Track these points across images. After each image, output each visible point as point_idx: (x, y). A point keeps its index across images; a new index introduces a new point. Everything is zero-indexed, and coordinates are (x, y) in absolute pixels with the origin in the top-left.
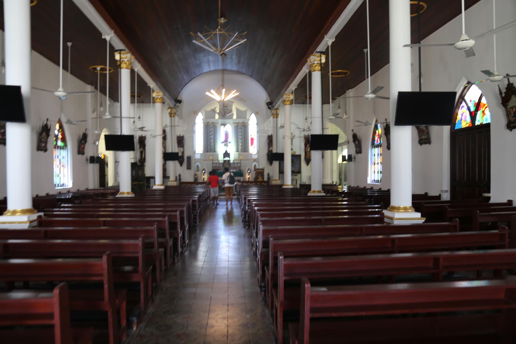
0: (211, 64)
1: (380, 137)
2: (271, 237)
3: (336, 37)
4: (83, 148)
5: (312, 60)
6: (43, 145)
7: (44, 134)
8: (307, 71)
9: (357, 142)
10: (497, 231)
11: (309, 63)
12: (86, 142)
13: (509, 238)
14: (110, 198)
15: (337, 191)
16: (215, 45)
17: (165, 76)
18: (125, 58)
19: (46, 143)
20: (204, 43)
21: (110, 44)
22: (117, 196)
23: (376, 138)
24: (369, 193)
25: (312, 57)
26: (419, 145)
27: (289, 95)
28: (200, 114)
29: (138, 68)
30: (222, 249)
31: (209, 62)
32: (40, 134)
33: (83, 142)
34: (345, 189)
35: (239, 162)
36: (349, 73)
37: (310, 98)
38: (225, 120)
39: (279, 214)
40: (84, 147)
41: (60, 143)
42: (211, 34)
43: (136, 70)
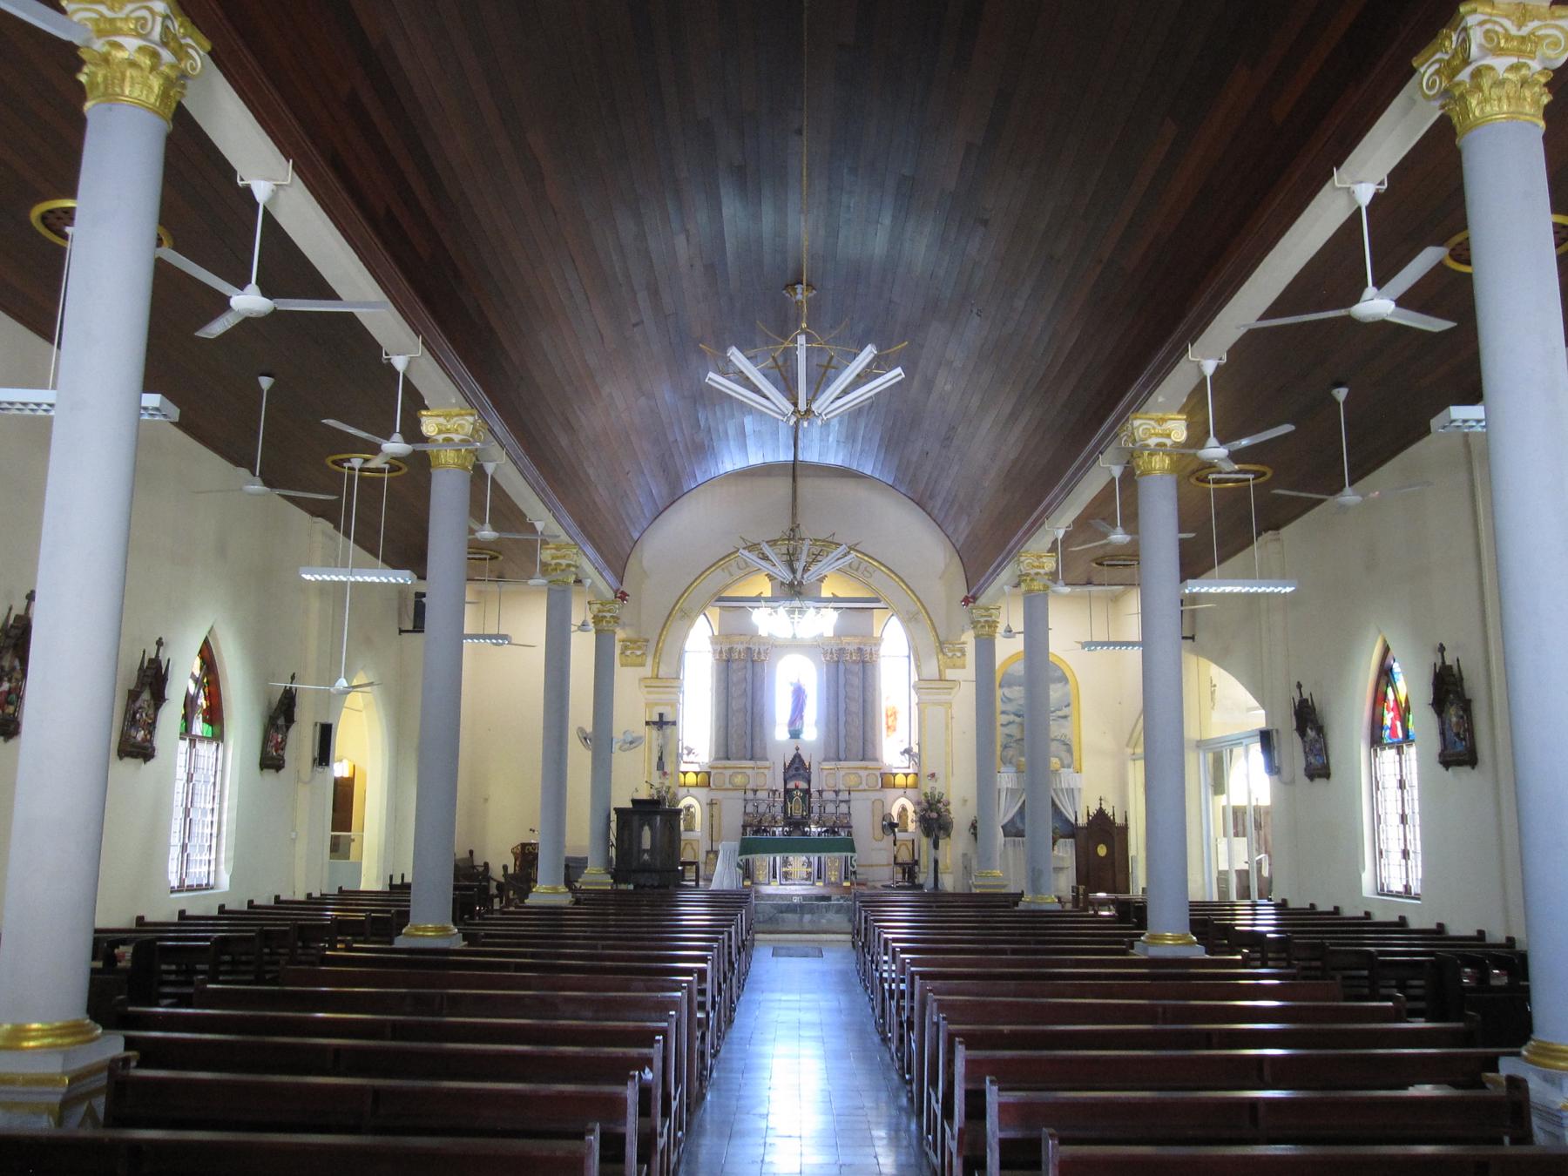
0: (750, 442)
1: (1403, 712)
2: (1052, 1136)
4: (281, 746)
6: (141, 735)
7: (146, 696)
8: (1117, 471)
10: (1461, 1025)
11: (1123, 440)
12: (290, 720)
14: (364, 949)
15: (1228, 930)
18: (450, 421)
19: (151, 727)
21: (407, 381)
22: (400, 942)
23: (1388, 718)
24: (1397, 949)
25: (1137, 423)
27: (1038, 553)
28: (701, 619)
29: (501, 465)
31: (742, 433)
32: (133, 696)
36: (1269, 475)
39: (1034, 1034)
40: (284, 740)
41: (199, 727)
43: (490, 468)
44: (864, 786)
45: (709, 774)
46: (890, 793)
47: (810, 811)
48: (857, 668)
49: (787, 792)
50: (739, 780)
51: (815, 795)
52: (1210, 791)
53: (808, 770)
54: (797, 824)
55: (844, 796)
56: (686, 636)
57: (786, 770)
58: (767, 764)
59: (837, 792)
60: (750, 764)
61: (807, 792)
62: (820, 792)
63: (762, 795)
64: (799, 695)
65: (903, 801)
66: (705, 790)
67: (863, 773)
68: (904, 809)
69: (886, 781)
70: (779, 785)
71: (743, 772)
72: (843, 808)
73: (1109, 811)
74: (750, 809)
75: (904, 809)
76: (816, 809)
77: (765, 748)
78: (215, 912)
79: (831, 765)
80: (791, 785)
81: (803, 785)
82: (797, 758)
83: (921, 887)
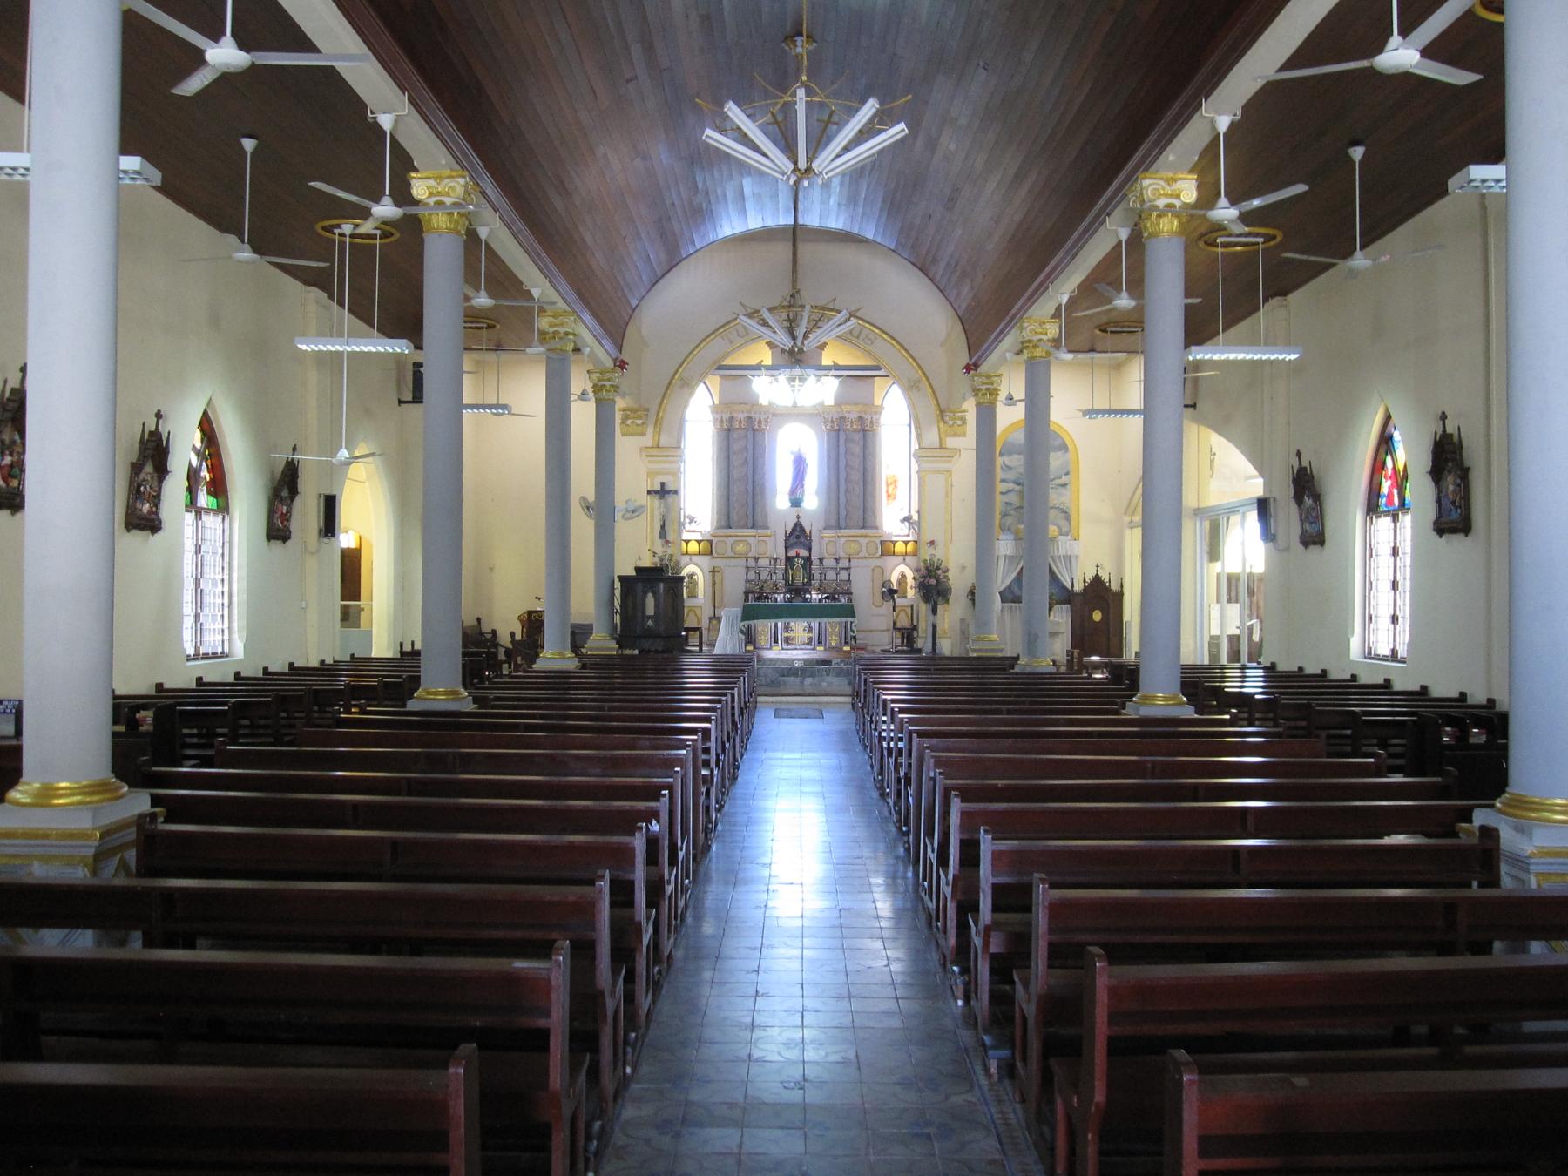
1: (1400, 481)
3: (1246, 108)
4: (286, 517)
5: (1148, 194)
7: (149, 468)
8: (1124, 234)
9: (1450, 483)
13: (1484, 949)
16: (789, 148)
17: (575, 267)
19: (156, 499)
20: (745, 140)
23: (1386, 486)
25: (1146, 183)
26: (1434, 535)
30: (804, 900)
33: (285, 493)
34: (1254, 685)
35: (1074, 532)
37: (632, 435)
38: (807, 414)
40: (289, 511)
42: (365, 214)
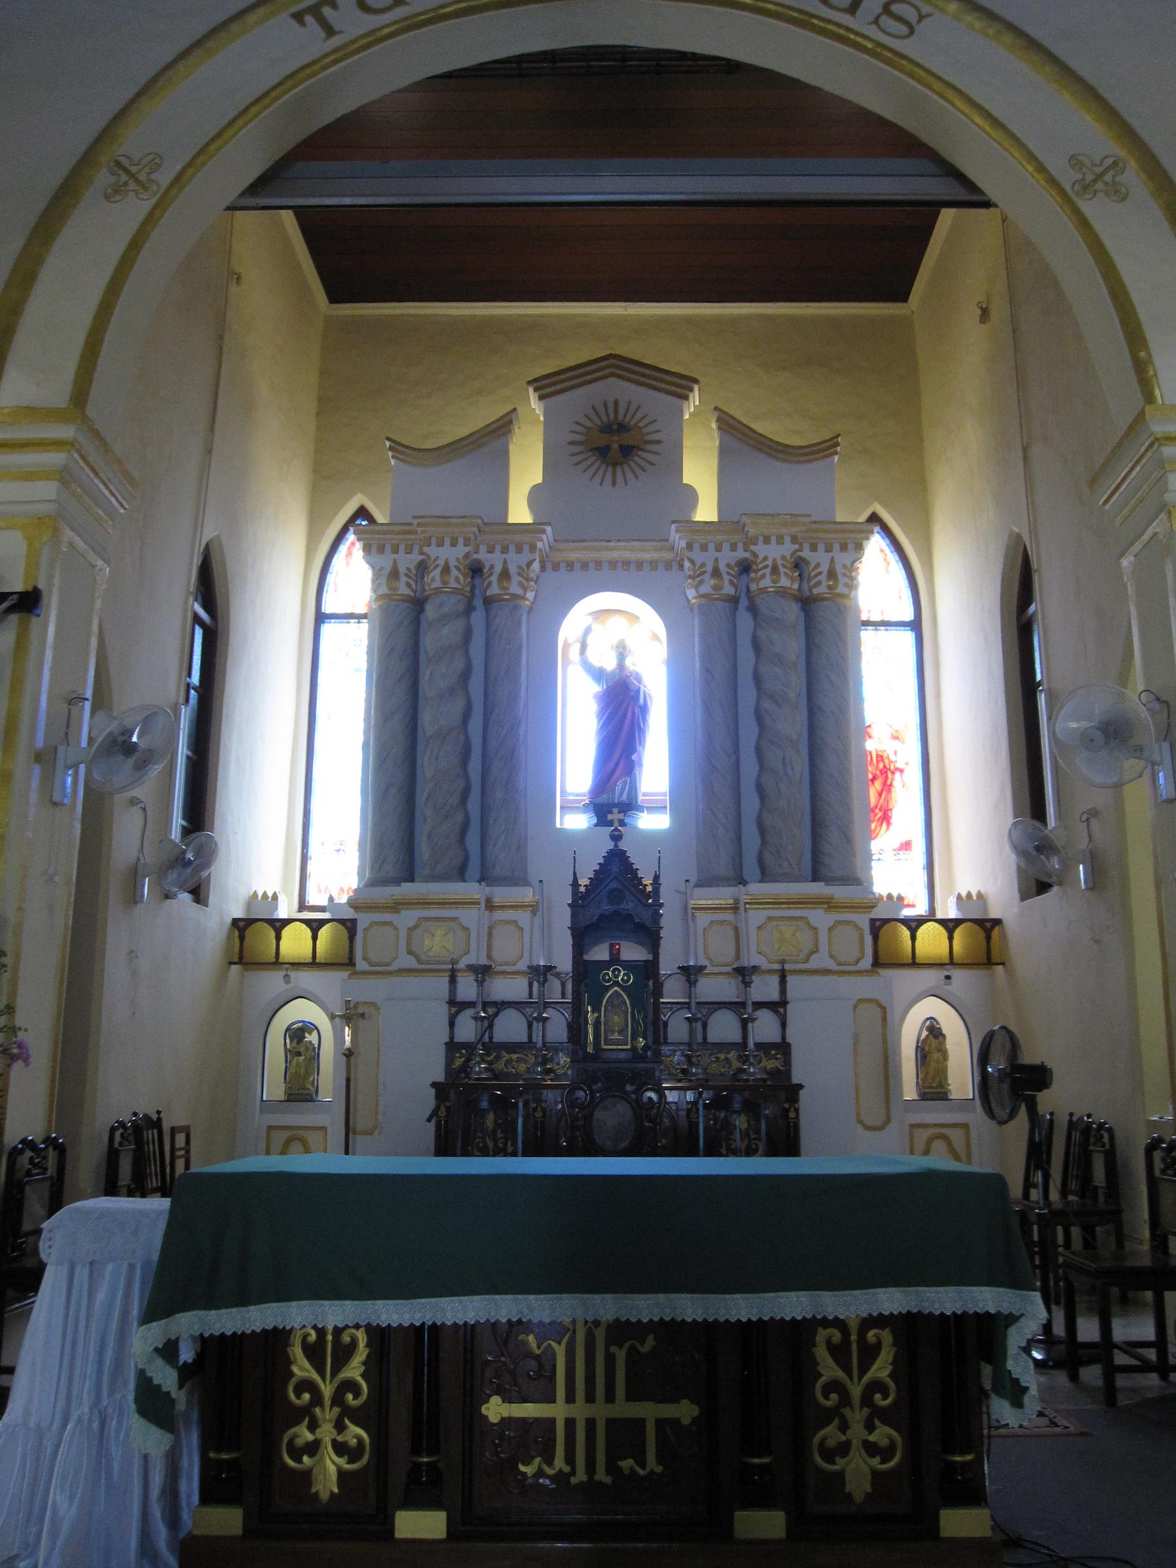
44: (821, 960)
45: (350, 926)
46: (903, 981)
47: (657, 1030)
48: (792, 612)
49: (586, 975)
50: (438, 943)
51: (673, 992)
52: (246, 159)
53: (650, 900)
54: (638, 1072)
55: (765, 988)
56: (561, 623)
57: (580, 901)
58: (527, 895)
59: (744, 974)
60: (471, 890)
61: (648, 971)
62: (690, 973)
63: (510, 988)
64: (621, 706)
65: (931, 1007)
66: (342, 975)
67: (821, 918)
68: (934, 1031)
69: (883, 938)
70: (564, 961)
71: (453, 920)
72: (765, 1028)
73: (848, 1477)
74: (467, 1030)
75: (934, 1031)
76: (678, 1028)
77: (521, 847)
78: (795, 1080)
79: (723, 895)
80: (600, 953)
81: (633, 952)
82: (617, 871)
83: (893, 1443)
